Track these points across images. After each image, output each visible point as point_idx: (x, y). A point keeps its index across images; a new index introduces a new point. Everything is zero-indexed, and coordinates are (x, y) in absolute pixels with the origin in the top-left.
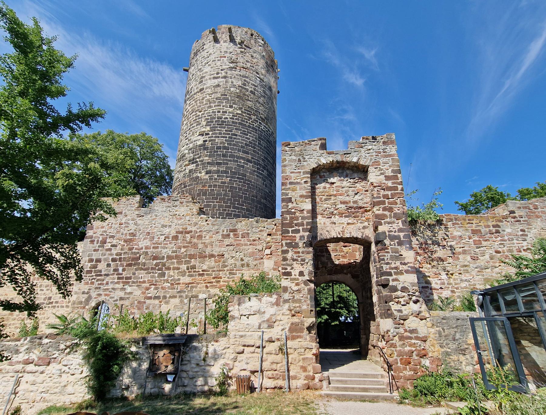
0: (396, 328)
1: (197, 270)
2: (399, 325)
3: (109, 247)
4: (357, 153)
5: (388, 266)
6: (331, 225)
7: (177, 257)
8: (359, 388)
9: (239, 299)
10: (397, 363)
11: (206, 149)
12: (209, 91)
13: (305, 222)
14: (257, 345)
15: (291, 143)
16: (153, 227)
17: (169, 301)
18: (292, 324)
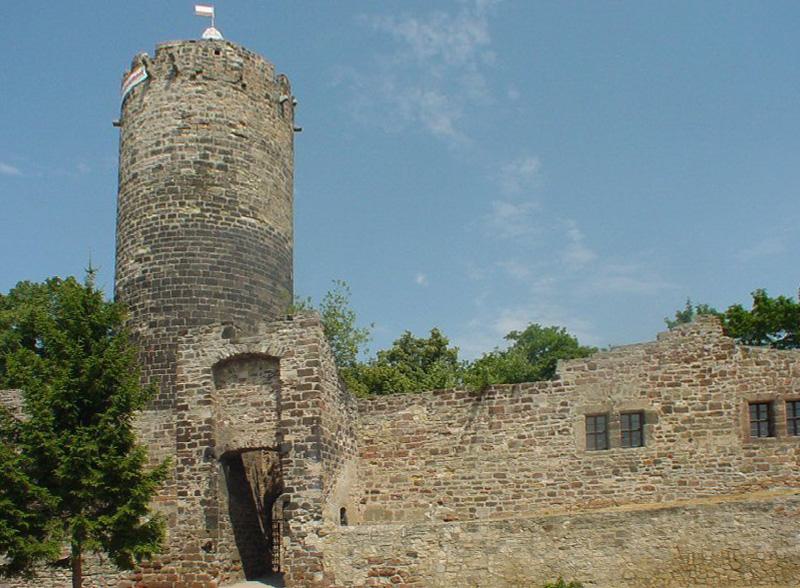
5: (290, 482)
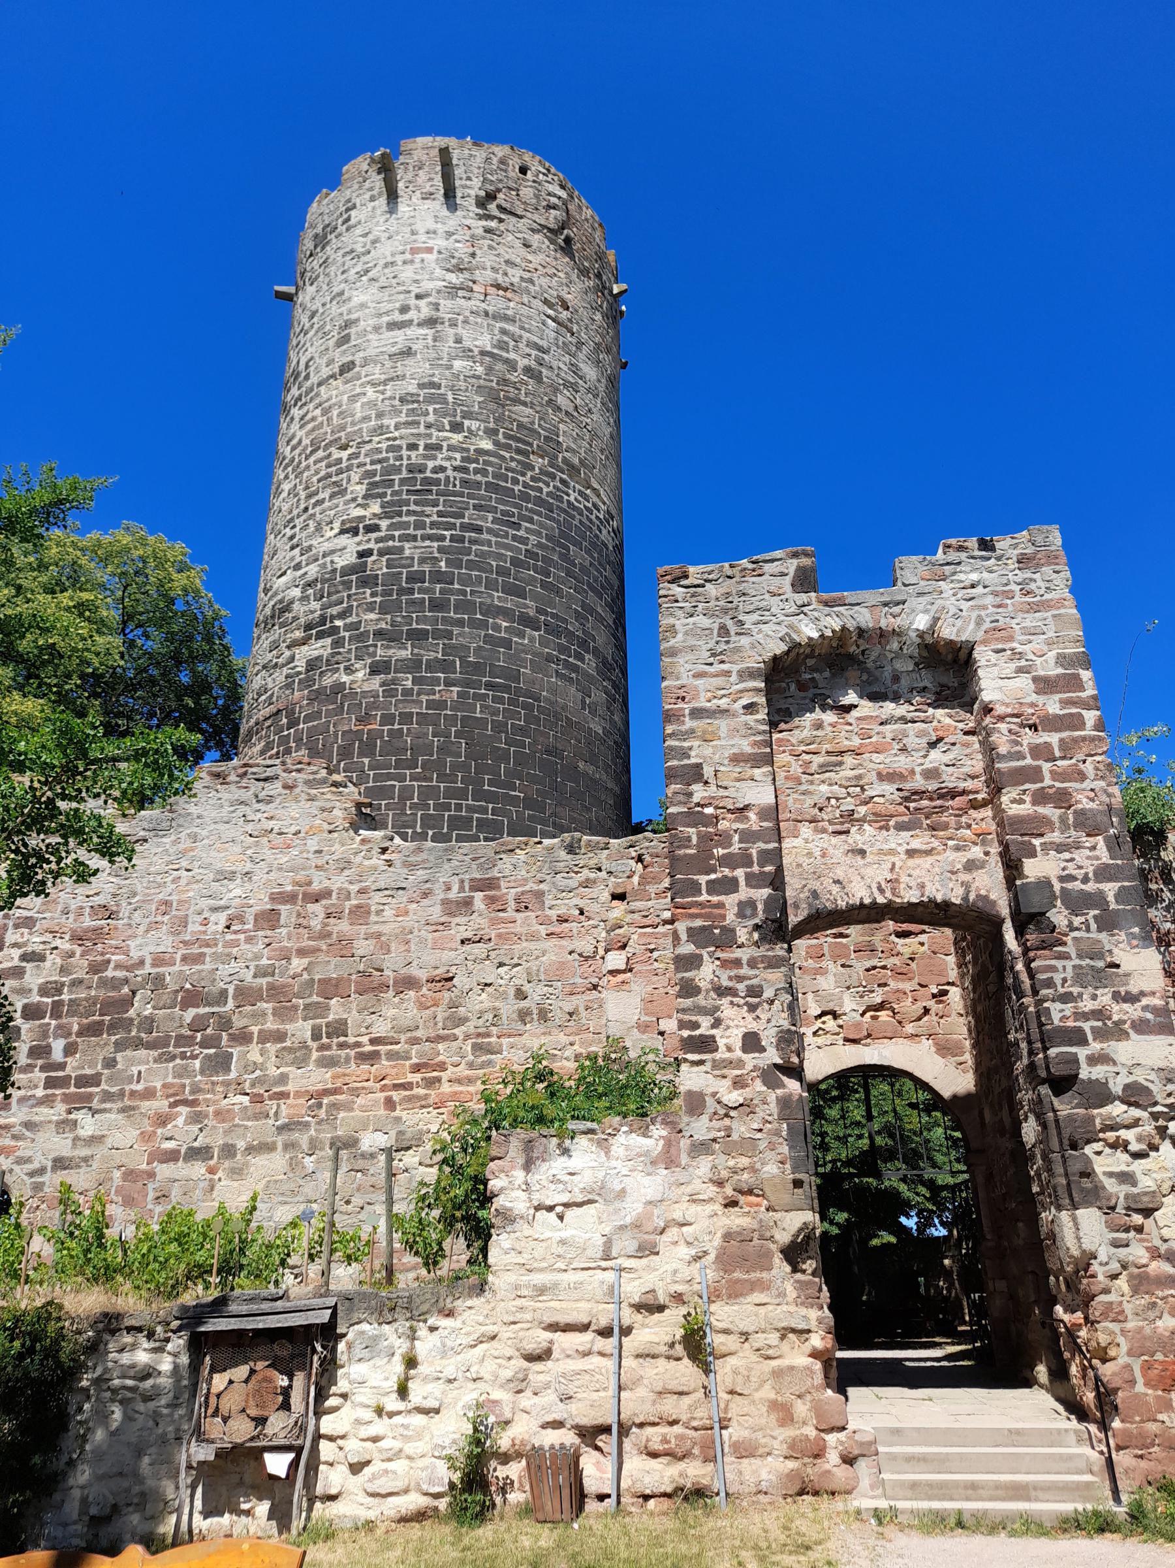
0: (1116, 1244)
1: (351, 1040)
2: (1127, 1230)
3: (16, 962)
4: (927, 598)
5: (1068, 1008)
6: (849, 859)
7: (275, 992)
8: (998, 1486)
9: (528, 1145)
10: (1133, 1382)
11: (367, 581)
12: (377, 373)
13: (754, 852)
14: (603, 1322)
15: (692, 569)
16: (183, 882)
17: (247, 1164)
18: (728, 1236)
